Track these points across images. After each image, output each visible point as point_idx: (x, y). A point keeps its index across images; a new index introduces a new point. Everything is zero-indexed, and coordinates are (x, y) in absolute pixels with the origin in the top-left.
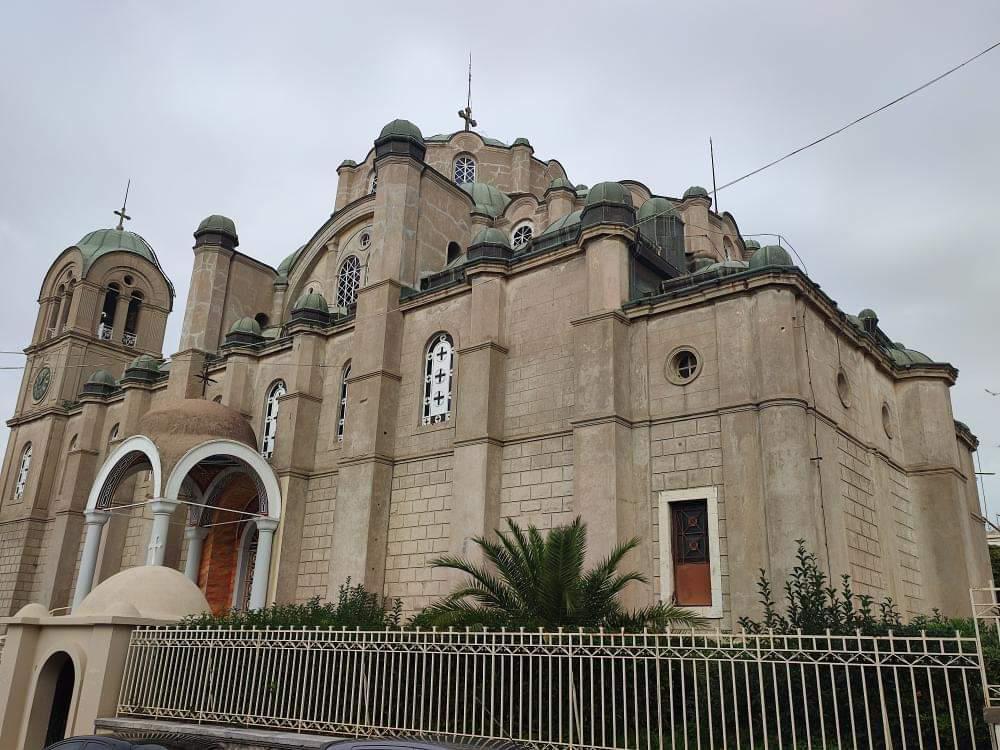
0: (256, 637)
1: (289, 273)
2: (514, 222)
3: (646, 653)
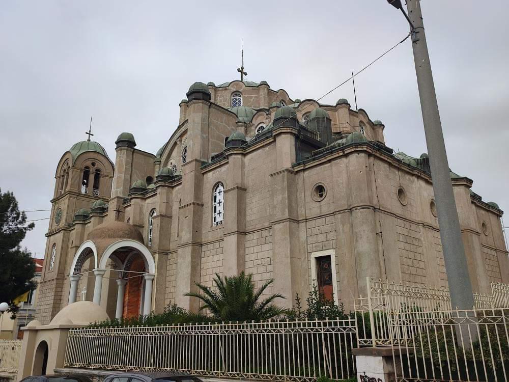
0: (192, 329)
1: (161, 156)
2: (256, 125)
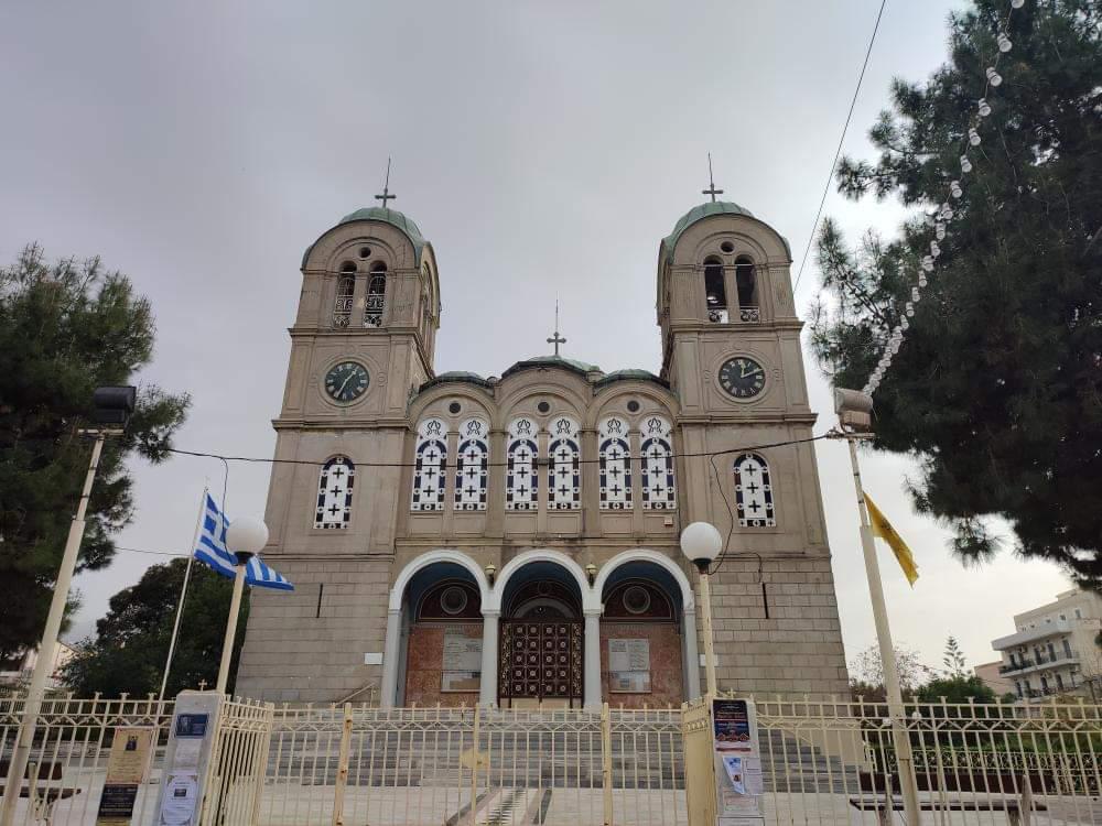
3: (92, 721)
